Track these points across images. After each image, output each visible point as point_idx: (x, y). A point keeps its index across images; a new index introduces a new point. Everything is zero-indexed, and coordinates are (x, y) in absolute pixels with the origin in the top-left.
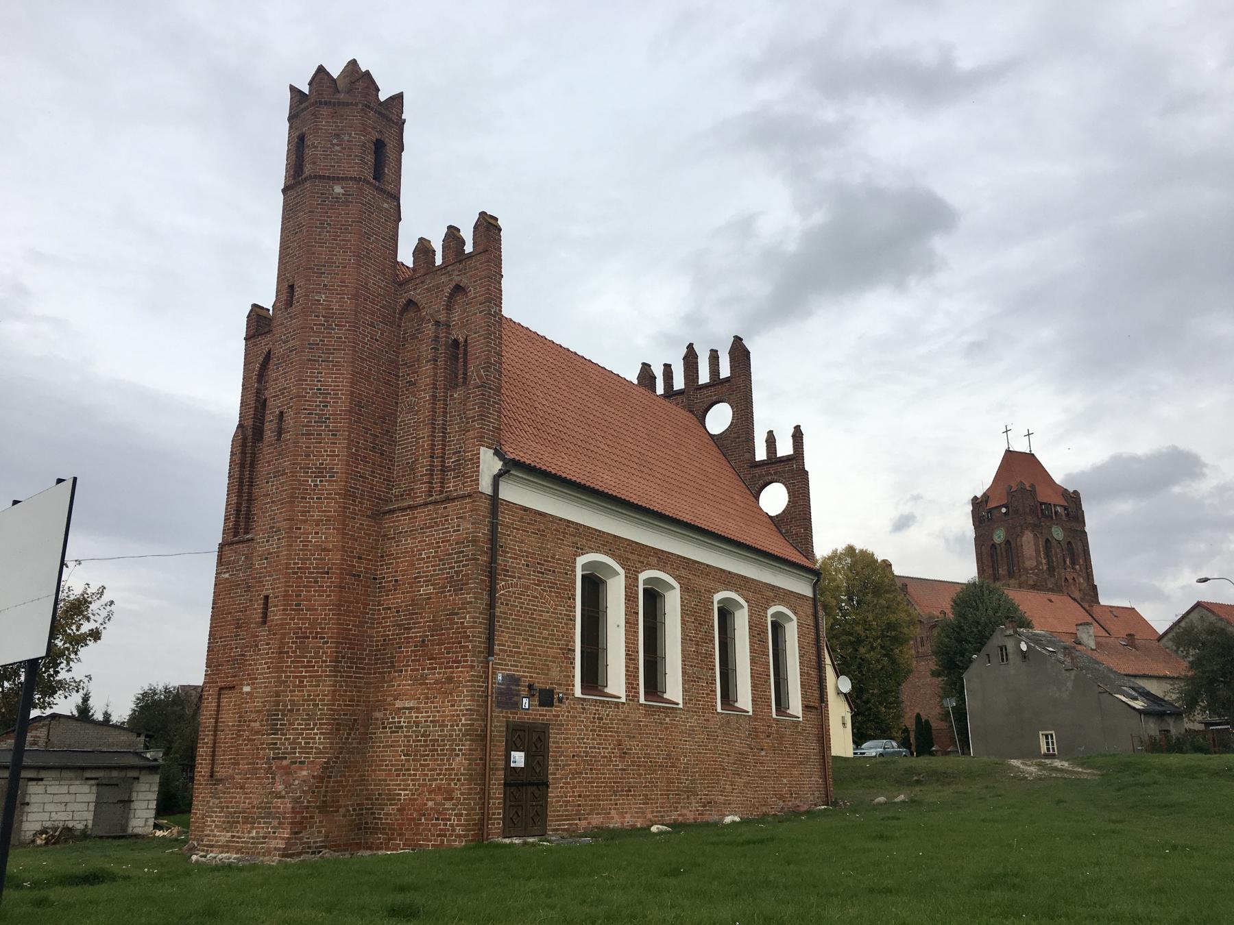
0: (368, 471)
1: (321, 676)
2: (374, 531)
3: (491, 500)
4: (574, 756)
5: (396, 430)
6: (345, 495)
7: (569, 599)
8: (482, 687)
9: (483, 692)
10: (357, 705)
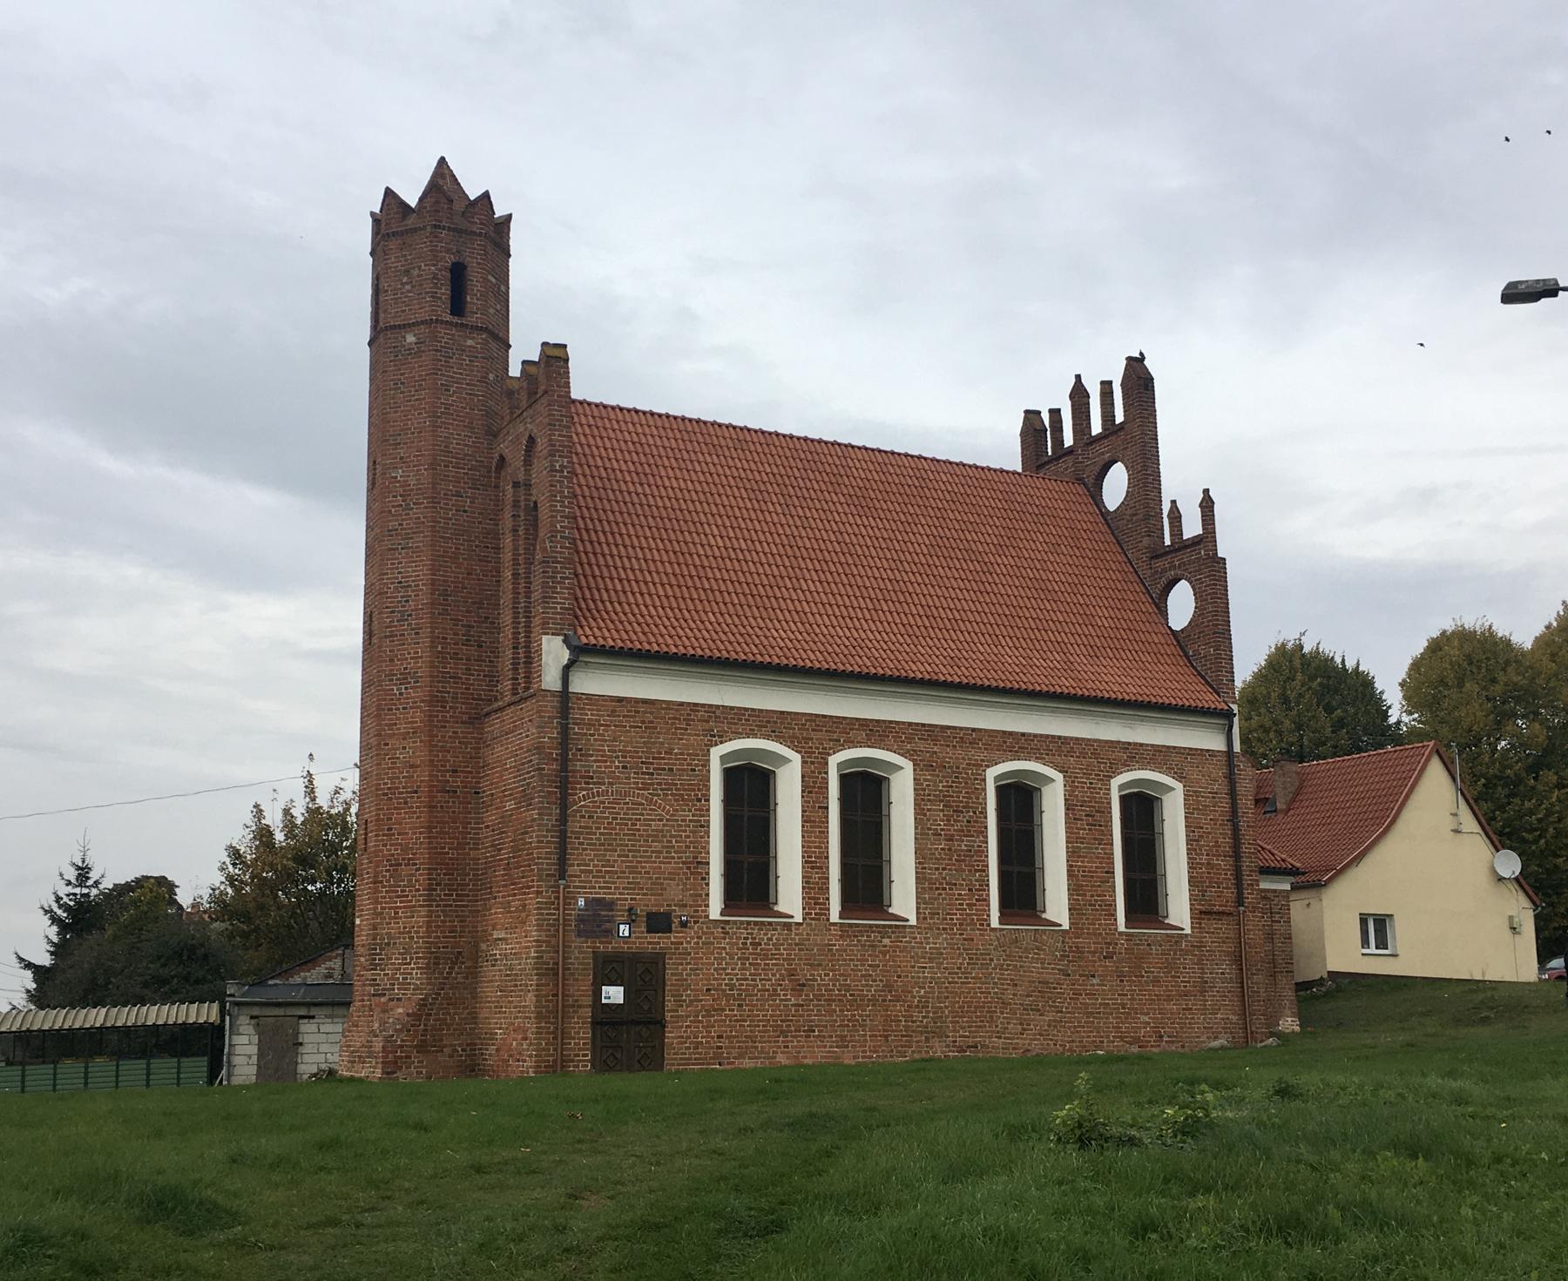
1: (414, 906)
2: (473, 738)
3: (561, 697)
4: (708, 990)
5: (499, 614)
6: (431, 701)
7: (699, 800)
8: (554, 914)
9: (554, 920)
10: (461, 937)
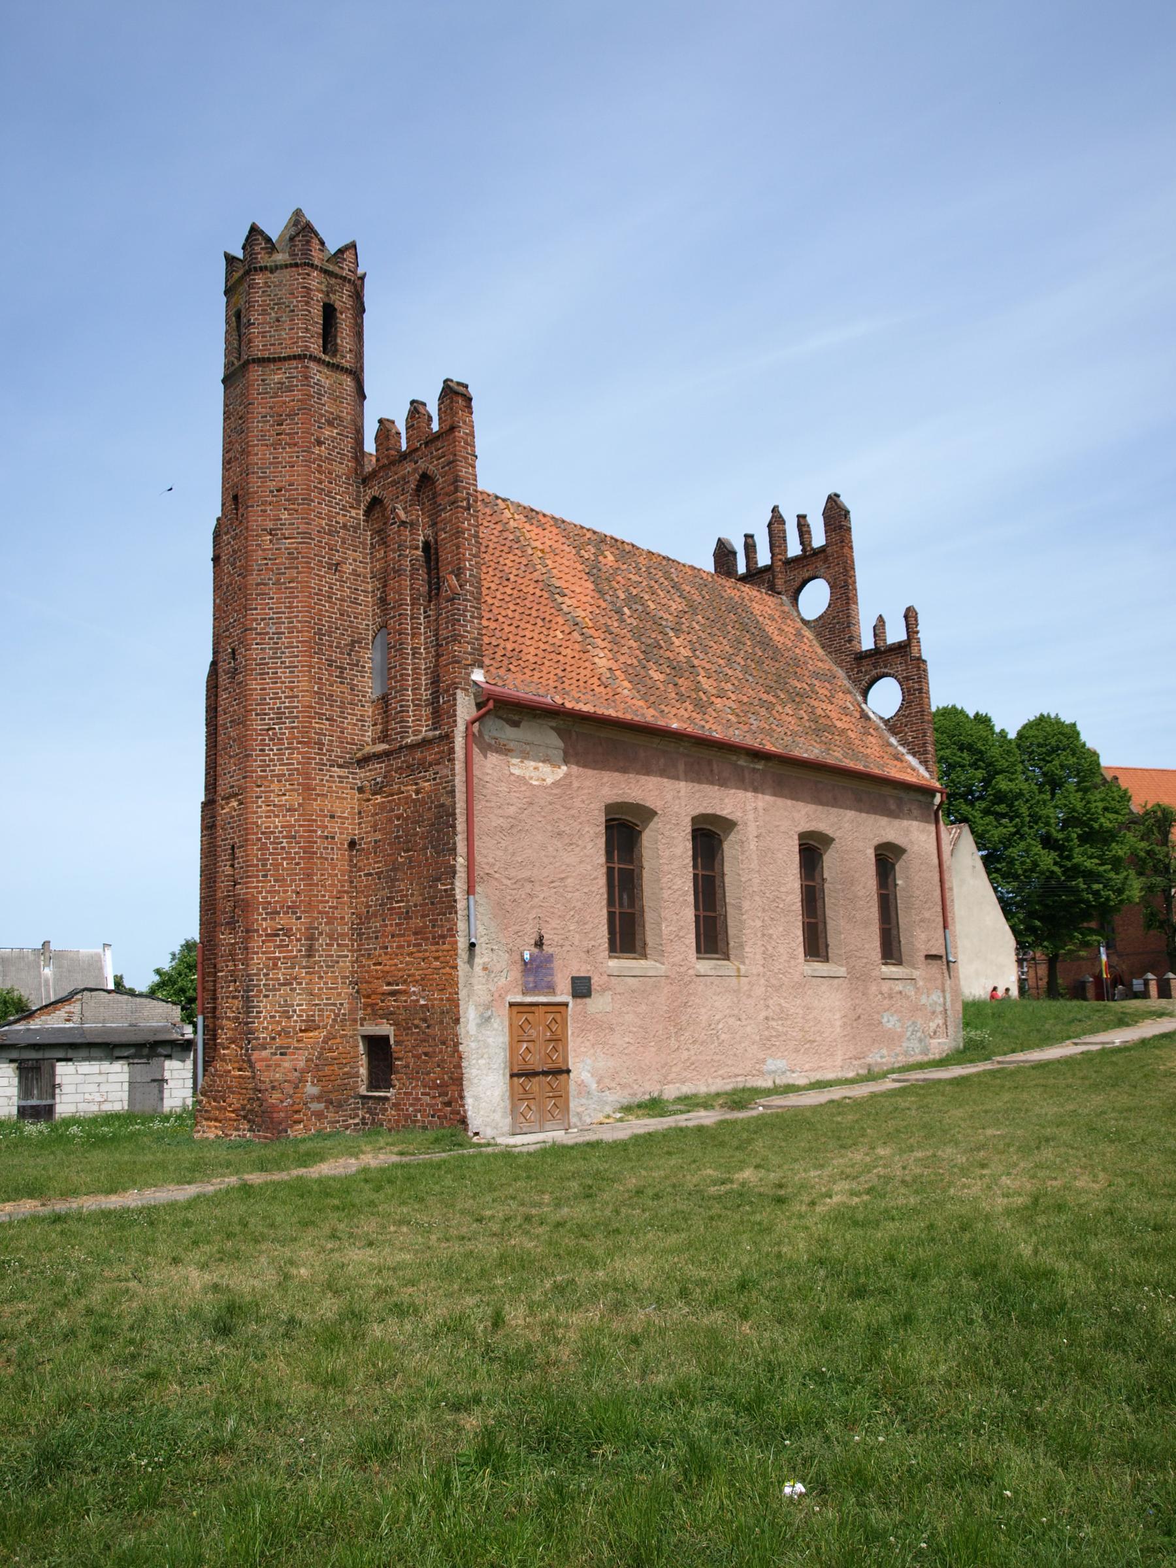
0: (336, 712)
